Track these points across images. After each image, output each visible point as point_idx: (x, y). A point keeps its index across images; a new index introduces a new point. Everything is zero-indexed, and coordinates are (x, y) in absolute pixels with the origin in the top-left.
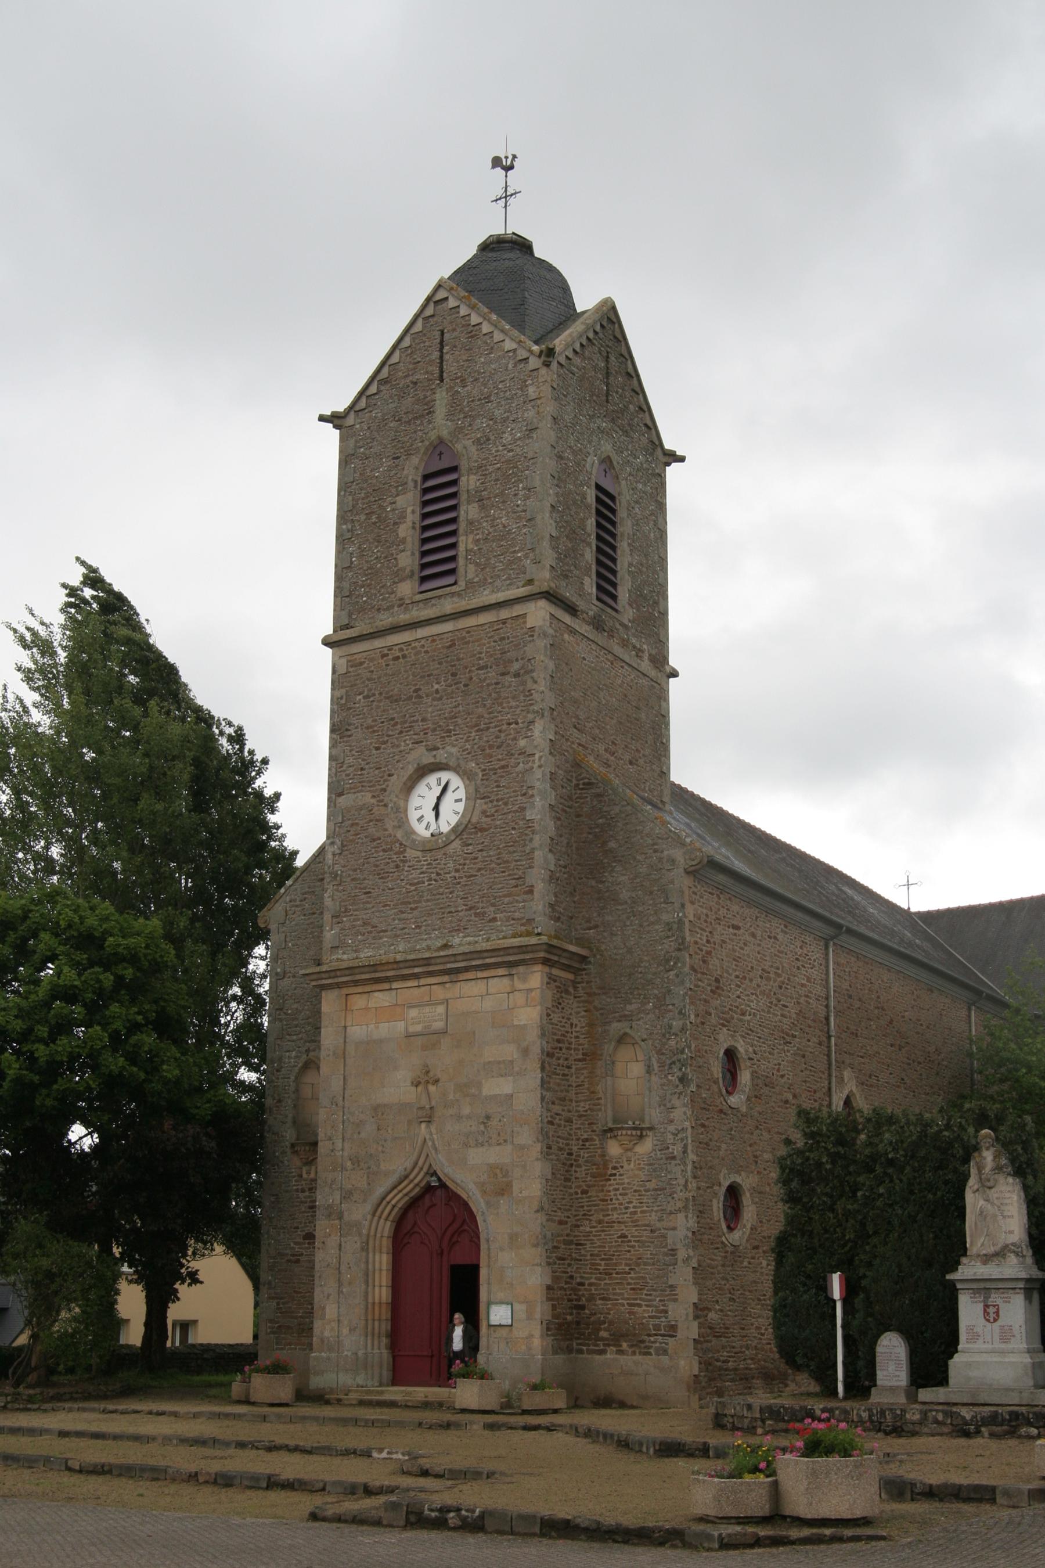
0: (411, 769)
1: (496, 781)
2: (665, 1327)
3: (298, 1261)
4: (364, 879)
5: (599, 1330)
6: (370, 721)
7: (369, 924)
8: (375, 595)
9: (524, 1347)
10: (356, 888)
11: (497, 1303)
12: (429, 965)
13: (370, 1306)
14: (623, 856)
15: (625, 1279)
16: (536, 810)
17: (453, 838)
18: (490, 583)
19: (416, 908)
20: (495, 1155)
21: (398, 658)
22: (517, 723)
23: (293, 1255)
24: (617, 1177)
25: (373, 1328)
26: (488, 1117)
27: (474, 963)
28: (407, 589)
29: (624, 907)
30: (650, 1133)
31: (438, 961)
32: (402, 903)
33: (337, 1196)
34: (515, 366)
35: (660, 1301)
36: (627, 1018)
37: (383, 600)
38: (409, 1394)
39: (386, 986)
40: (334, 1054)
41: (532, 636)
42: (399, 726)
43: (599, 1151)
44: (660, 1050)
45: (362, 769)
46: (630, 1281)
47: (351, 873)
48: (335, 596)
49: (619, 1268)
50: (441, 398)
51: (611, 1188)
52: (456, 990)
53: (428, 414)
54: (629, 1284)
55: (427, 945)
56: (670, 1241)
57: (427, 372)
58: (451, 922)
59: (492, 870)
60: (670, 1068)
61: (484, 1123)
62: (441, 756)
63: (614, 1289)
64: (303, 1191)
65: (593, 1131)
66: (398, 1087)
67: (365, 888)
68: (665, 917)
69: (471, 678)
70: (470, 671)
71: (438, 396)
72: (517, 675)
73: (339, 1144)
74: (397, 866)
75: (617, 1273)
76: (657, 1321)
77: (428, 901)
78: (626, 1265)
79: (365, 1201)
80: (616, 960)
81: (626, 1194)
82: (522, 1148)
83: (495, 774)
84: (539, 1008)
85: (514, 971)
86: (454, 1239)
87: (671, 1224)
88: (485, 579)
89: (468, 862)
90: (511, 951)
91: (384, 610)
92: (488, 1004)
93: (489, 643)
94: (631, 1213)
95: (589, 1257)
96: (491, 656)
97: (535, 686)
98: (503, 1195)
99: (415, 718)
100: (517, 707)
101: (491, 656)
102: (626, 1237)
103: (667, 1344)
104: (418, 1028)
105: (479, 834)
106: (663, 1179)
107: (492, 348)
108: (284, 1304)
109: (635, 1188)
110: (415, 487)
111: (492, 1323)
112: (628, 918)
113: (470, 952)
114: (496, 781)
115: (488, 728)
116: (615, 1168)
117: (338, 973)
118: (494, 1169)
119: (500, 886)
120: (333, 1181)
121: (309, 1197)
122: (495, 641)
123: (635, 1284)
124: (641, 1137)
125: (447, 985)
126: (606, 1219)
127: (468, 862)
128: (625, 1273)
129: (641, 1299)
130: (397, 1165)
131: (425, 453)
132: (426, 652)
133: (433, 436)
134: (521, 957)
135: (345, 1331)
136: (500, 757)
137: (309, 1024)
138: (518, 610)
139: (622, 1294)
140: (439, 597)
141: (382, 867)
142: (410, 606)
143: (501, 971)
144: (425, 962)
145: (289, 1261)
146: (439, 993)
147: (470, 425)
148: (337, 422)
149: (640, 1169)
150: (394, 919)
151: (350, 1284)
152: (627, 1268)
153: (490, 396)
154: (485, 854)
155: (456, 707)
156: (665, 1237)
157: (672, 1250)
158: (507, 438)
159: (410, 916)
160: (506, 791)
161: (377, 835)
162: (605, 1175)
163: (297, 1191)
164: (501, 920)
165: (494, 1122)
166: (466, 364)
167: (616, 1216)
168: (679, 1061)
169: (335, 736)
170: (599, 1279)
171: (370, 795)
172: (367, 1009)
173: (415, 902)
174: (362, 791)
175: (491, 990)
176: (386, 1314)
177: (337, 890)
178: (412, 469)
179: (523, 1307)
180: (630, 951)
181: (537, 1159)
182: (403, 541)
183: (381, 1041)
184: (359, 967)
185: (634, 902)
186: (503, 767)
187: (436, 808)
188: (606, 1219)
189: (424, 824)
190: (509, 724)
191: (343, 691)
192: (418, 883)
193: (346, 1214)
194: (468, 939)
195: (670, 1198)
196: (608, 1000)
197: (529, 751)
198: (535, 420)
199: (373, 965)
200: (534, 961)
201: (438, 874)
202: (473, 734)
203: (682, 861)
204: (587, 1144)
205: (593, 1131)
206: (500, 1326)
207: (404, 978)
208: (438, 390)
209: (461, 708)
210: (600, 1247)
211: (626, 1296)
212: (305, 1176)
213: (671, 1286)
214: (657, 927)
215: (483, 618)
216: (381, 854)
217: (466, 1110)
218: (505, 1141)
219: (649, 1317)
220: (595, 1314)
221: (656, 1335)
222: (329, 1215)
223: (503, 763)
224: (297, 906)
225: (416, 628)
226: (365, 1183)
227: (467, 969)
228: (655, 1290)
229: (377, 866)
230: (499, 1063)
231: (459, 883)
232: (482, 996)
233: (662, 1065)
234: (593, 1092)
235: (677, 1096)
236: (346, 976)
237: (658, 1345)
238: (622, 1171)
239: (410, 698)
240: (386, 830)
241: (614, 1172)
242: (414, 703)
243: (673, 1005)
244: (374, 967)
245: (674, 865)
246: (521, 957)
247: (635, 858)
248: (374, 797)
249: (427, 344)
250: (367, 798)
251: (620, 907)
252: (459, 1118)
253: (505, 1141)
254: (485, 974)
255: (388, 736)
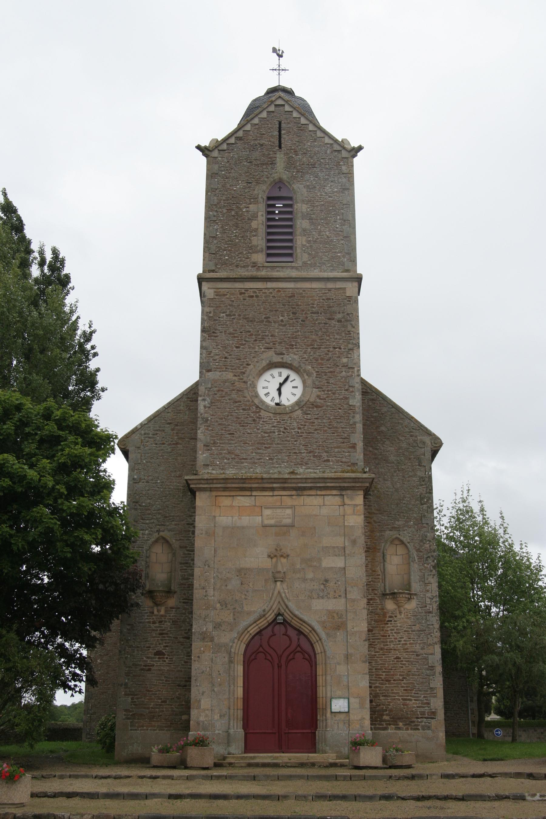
0: (264, 363)
1: (326, 380)
2: (428, 713)
3: (149, 670)
4: (229, 425)
5: (383, 715)
6: (231, 330)
7: (233, 453)
8: (235, 257)
9: (358, 726)
10: (222, 430)
11: (336, 698)
12: (285, 483)
13: (236, 699)
14: (390, 436)
15: (400, 684)
16: (356, 400)
17: (297, 408)
18: (319, 266)
19: (269, 447)
20: (332, 604)
21: (252, 297)
22: (340, 348)
23: (145, 666)
24: (393, 622)
25: (237, 715)
26: (327, 581)
27: (318, 485)
28: (260, 258)
29: (393, 465)
30: (415, 597)
31: (293, 481)
32: (258, 443)
33: (210, 627)
34: (332, 152)
35: (424, 697)
36: (397, 529)
37: (241, 261)
38: (276, 758)
39: (248, 493)
40: (206, 533)
41: (350, 301)
42: (254, 337)
43: (380, 606)
44: (419, 549)
45: (226, 358)
46: (403, 685)
47: (218, 420)
48: (204, 251)
49: (395, 677)
50: (280, 159)
51: (389, 629)
52: (301, 500)
53: (271, 164)
54: (402, 687)
55: (281, 470)
56: (430, 661)
57: (270, 141)
58: (296, 459)
59: (325, 431)
60: (427, 560)
61: (324, 584)
62: (287, 358)
63: (392, 690)
64: (154, 623)
65: (375, 594)
66: (257, 557)
67: (229, 431)
68: (419, 473)
69: (307, 318)
70: (306, 313)
71: (278, 155)
72: (339, 321)
73: (211, 592)
74: (254, 420)
75: (394, 680)
76: (422, 709)
77: (278, 444)
78: (400, 675)
79: (231, 630)
80: (388, 494)
81: (399, 633)
82: (353, 601)
83: (325, 375)
84: (363, 516)
85: (344, 493)
86: (253, 657)
87: (430, 652)
88: (316, 264)
89: (307, 424)
90: (347, 480)
91: (241, 267)
92: (325, 511)
93: (319, 299)
94: (403, 644)
95: (374, 671)
96: (321, 307)
97: (353, 329)
98: (339, 629)
99: (266, 334)
100: (340, 339)
101: (321, 307)
102: (400, 658)
103: (429, 723)
104: (272, 522)
105: (315, 409)
106: (424, 625)
107: (315, 139)
108: (137, 699)
109: (405, 629)
110: (263, 202)
111: (333, 711)
112: (395, 472)
113: (319, 478)
114: (326, 380)
115: (320, 348)
116: (391, 617)
117: (215, 481)
118: (331, 613)
119: (331, 441)
120: (207, 616)
121: (159, 627)
122: (323, 300)
123: (407, 687)
124: (409, 599)
125: (294, 497)
126: (386, 647)
127: (307, 424)
128: (400, 680)
129: (411, 696)
130: (257, 608)
131: (270, 185)
132: (274, 297)
133: (276, 176)
134: (353, 485)
135: (217, 717)
136: (329, 366)
137: (159, 514)
138: (339, 285)
139: (398, 693)
140: (282, 267)
141: (242, 419)
142: (261, 269)
143: (334, 492)
144: (284, 481)
145: (142, 669)
146: (288, 501)
147: (302, 177)
148: (207, 152)
149: (408, 618)
150: (252, 453)
151: (220, 685)
152: (401, 678)
153: (315, 164)
154: (319, 421)
155: (296, 332)
156: (427, 659)
157: (432, 667)
158: (328, 189)
159: (264, 452)
160: (334, 386)
161: (238, 399)
162: (385, 620)
163: (149, 622)
164: (332, 461)
165: (331, 584)
166: (297, 144)
167: (392, 646)
168: (432, 556)
169: (204, 335)
170: (382, 684)
171: (232, 374)
172: (232, 506)
173: (268, 444)
174: (225, 371)
175: (327, 503)
176: (240, 704)
177: (207, 429)
178: (262, 191)
179: (357, 700)
180: (397, 490)
181: (364, 608)
182: (256, 230)
183: (243, 527)
184: (234, 479)
185: (399, 463)
186: (331, 372)
187: (279, 390)
188: (386, 647)
189: (270, 398)
190: (335, 348)
191: (212, 309)
192: (271, 432)
193: (216, 638)
194: (309, 470)
195: (429, 636)
196: (383, 517)
197: (350, 365)
198: (347, 184)
199: (245, 479)
200: (359, 488)
201: (285, 429)
202: (309, 350)
203: (430, 443)
204: (371, 602)
205: (375, 594)
206: (340, 712)
207: (264, 489)
208: (278, 153)
209: (299, 333)
210: (381, 664)
211: (401, 694)
212: (156, 612)
213: (431, 688)
214: (414, 479)
215: (315, 285)
216: (241, 411)
217: (310, 575)
218: (340, 596)
219: (417, 707)
220: (380, 705)
221: (422, 718)
222: (204, 638)
223: (331, 370)
224: (149, 438)
225: (267, 281)
226: (232, 618)
227: (311, 488)
228: (420, 691)
229: (238, 418)
230: (334, 547)
231: (302, 436)
232: (321, 507)
233: (420, 558)
234: (374, 571)
235: (432, 576)
236: (220, 483)
237: (423, 724)
238: (395, 619)
239: (262, 321)
240: (245, 397)
241: (390, 619)
242: (265, 325)
243: (427, 524)
244: (244, 480)
245: (424, 445)
246: (353, 485)
247: (398, 438)
248: (235, 376)
249: (269, 126)
250: (229, 376)
251: (389, 465)
252: (305, 580)
253: (340, 596)
254: (323, 493)
255: (245, 341)
